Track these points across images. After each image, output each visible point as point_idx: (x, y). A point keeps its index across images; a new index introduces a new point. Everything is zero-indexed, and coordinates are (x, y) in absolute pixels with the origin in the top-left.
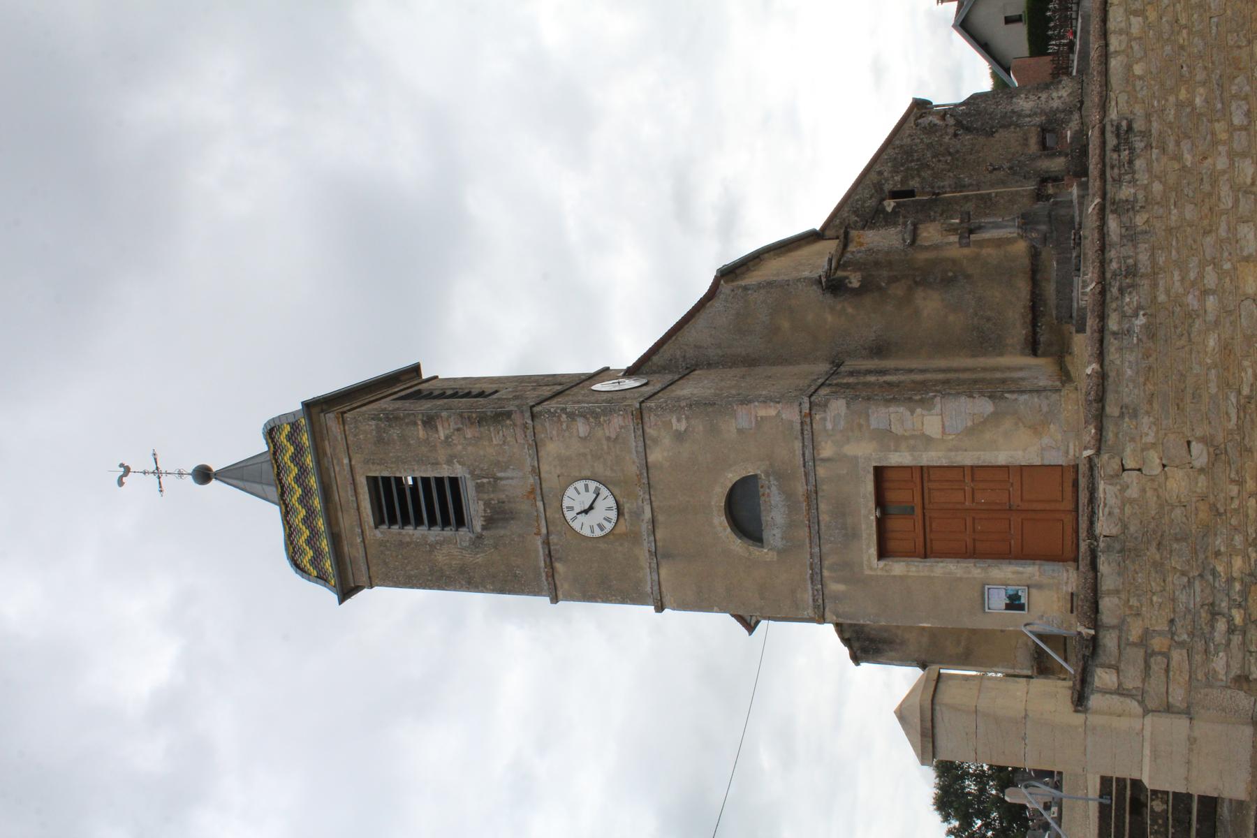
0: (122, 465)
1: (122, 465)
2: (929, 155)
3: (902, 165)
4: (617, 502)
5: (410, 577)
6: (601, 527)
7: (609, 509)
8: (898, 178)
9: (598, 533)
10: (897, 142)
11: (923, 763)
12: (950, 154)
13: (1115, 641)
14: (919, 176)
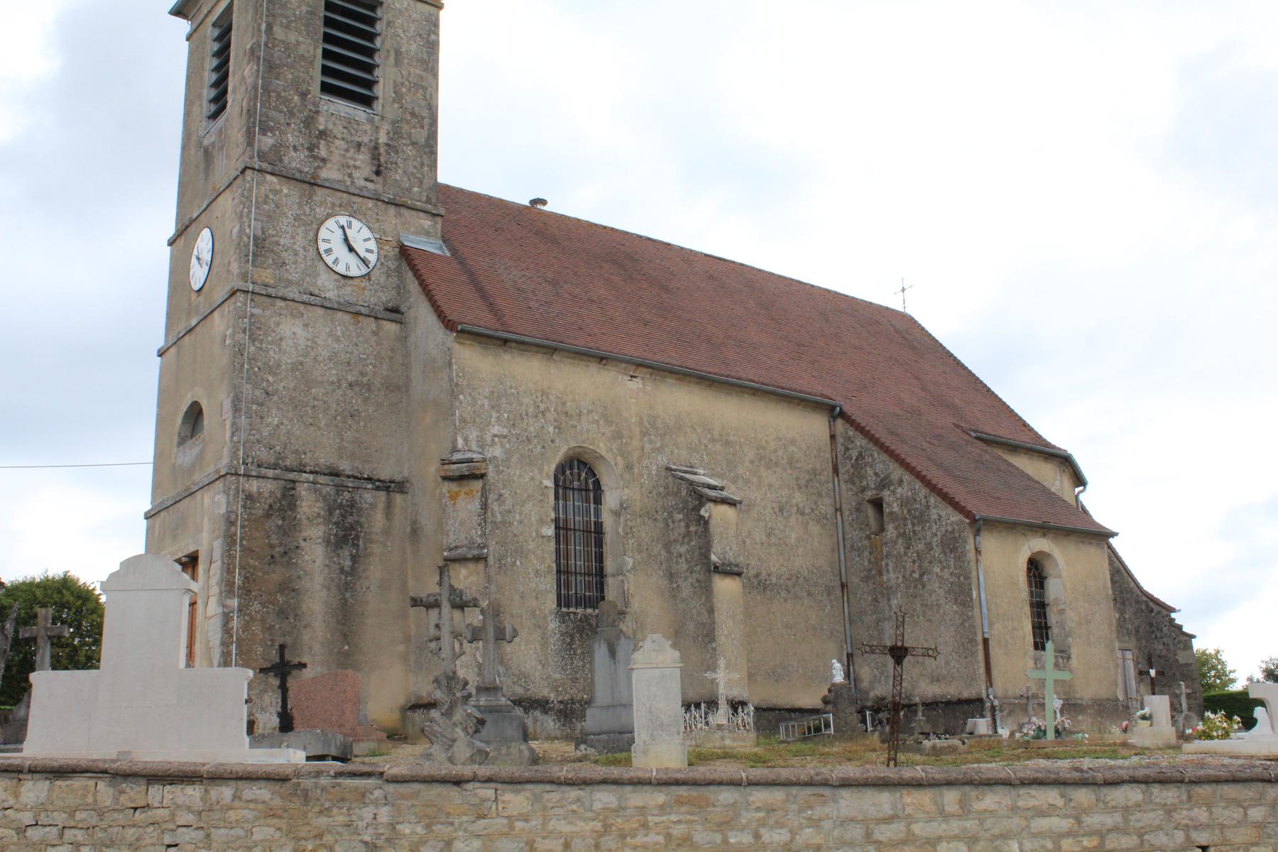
2: (921, 547)
3: (909, 511)
4: (352, 278)
6: (329, 251)
8: (896, 508)
9: (323, 246)
10: (932, 500)
11: (122, 564)
12: (921, 576)
13: (883, 827)
14: (898, 536)
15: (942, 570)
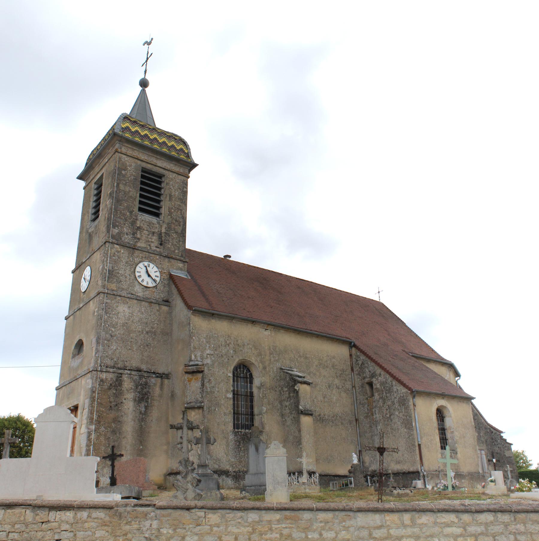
0: (144, 45)
1: (144, 45)
2: (390, 403)
3: (384, 387)
5: (90, 236)
6: (140, 276)
7: (147, 283)
9: (137, 274)
12: (390, 416)
14: (380, 398)
15: (399, 413)
